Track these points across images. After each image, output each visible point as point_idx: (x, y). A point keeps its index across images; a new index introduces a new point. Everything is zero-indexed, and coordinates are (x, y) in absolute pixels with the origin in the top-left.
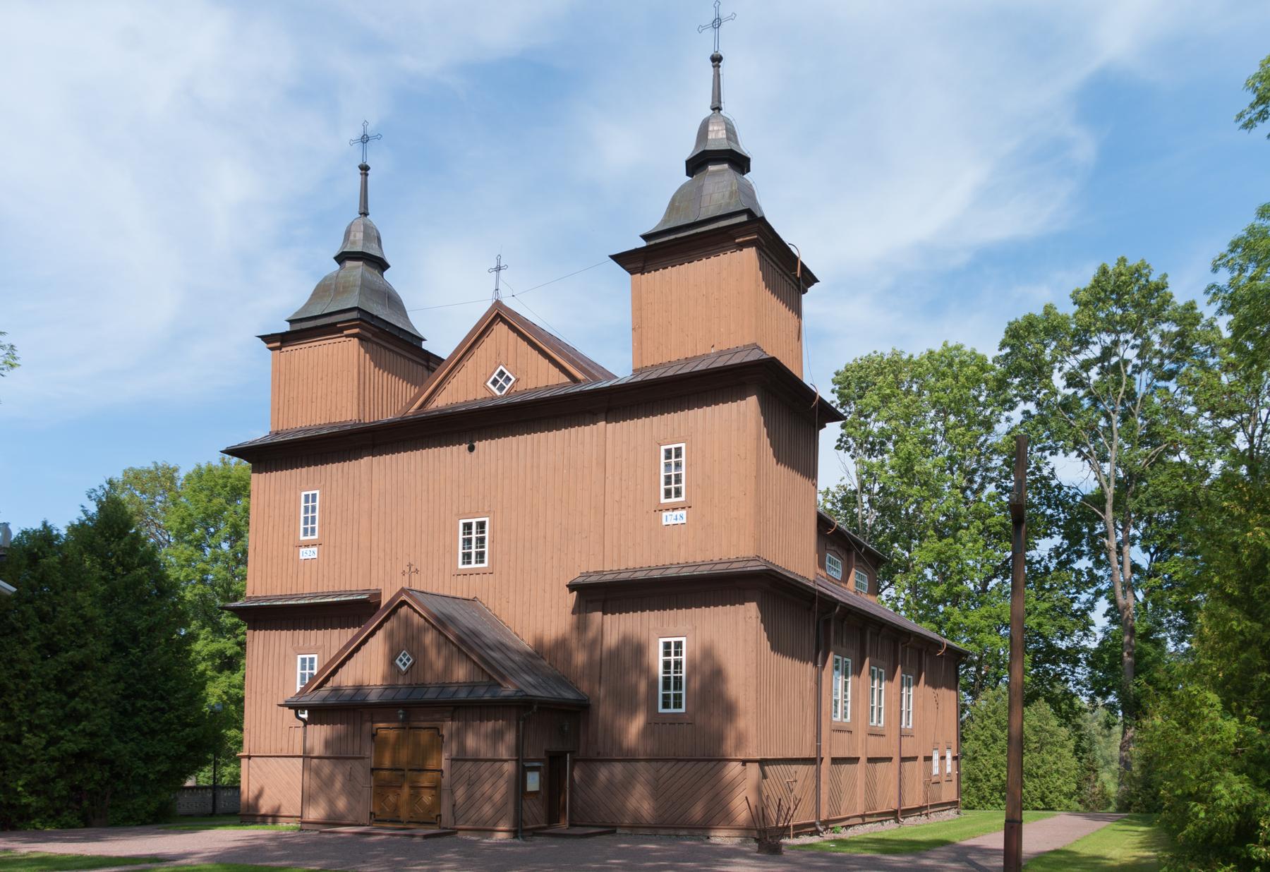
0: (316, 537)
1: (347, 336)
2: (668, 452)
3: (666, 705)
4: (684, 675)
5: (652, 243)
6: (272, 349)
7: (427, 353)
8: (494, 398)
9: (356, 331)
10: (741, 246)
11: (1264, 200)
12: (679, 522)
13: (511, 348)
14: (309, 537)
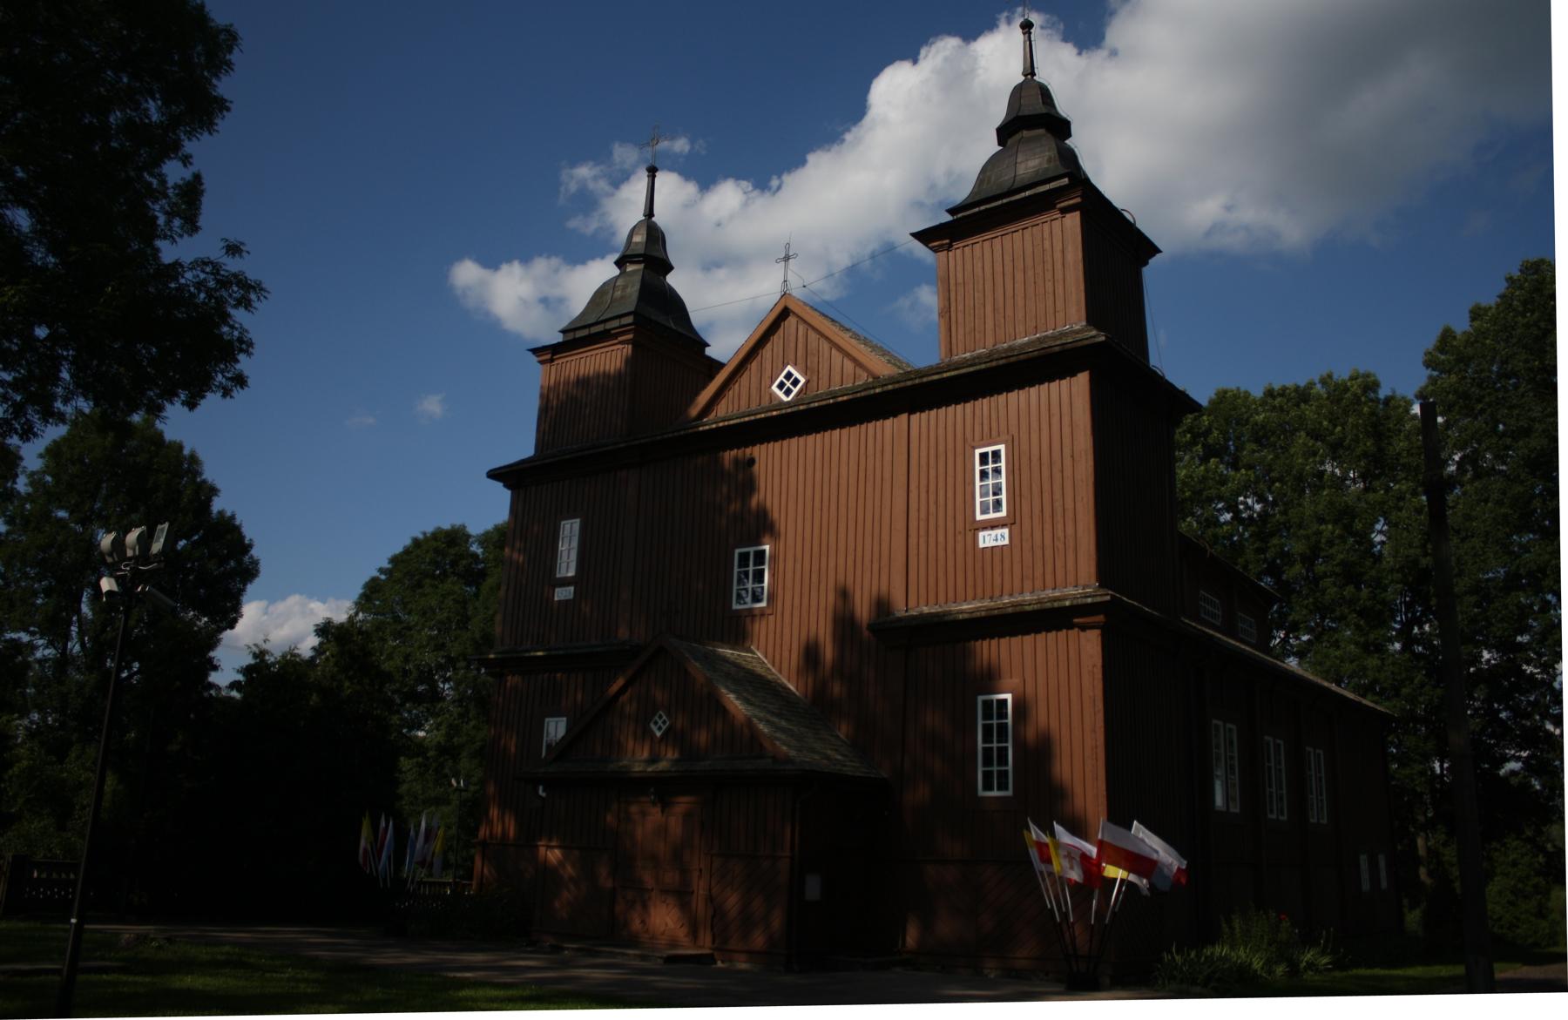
0: (1003, 513)
2: (984, 457)
3: (988, 787)
4: (1010, 720)
6: (541, 362)
7: (709, 359)
8: (782, 404)
10: (1064, 211)
12: (1000, 543)
13: (801, 339)
14: (992, 515)
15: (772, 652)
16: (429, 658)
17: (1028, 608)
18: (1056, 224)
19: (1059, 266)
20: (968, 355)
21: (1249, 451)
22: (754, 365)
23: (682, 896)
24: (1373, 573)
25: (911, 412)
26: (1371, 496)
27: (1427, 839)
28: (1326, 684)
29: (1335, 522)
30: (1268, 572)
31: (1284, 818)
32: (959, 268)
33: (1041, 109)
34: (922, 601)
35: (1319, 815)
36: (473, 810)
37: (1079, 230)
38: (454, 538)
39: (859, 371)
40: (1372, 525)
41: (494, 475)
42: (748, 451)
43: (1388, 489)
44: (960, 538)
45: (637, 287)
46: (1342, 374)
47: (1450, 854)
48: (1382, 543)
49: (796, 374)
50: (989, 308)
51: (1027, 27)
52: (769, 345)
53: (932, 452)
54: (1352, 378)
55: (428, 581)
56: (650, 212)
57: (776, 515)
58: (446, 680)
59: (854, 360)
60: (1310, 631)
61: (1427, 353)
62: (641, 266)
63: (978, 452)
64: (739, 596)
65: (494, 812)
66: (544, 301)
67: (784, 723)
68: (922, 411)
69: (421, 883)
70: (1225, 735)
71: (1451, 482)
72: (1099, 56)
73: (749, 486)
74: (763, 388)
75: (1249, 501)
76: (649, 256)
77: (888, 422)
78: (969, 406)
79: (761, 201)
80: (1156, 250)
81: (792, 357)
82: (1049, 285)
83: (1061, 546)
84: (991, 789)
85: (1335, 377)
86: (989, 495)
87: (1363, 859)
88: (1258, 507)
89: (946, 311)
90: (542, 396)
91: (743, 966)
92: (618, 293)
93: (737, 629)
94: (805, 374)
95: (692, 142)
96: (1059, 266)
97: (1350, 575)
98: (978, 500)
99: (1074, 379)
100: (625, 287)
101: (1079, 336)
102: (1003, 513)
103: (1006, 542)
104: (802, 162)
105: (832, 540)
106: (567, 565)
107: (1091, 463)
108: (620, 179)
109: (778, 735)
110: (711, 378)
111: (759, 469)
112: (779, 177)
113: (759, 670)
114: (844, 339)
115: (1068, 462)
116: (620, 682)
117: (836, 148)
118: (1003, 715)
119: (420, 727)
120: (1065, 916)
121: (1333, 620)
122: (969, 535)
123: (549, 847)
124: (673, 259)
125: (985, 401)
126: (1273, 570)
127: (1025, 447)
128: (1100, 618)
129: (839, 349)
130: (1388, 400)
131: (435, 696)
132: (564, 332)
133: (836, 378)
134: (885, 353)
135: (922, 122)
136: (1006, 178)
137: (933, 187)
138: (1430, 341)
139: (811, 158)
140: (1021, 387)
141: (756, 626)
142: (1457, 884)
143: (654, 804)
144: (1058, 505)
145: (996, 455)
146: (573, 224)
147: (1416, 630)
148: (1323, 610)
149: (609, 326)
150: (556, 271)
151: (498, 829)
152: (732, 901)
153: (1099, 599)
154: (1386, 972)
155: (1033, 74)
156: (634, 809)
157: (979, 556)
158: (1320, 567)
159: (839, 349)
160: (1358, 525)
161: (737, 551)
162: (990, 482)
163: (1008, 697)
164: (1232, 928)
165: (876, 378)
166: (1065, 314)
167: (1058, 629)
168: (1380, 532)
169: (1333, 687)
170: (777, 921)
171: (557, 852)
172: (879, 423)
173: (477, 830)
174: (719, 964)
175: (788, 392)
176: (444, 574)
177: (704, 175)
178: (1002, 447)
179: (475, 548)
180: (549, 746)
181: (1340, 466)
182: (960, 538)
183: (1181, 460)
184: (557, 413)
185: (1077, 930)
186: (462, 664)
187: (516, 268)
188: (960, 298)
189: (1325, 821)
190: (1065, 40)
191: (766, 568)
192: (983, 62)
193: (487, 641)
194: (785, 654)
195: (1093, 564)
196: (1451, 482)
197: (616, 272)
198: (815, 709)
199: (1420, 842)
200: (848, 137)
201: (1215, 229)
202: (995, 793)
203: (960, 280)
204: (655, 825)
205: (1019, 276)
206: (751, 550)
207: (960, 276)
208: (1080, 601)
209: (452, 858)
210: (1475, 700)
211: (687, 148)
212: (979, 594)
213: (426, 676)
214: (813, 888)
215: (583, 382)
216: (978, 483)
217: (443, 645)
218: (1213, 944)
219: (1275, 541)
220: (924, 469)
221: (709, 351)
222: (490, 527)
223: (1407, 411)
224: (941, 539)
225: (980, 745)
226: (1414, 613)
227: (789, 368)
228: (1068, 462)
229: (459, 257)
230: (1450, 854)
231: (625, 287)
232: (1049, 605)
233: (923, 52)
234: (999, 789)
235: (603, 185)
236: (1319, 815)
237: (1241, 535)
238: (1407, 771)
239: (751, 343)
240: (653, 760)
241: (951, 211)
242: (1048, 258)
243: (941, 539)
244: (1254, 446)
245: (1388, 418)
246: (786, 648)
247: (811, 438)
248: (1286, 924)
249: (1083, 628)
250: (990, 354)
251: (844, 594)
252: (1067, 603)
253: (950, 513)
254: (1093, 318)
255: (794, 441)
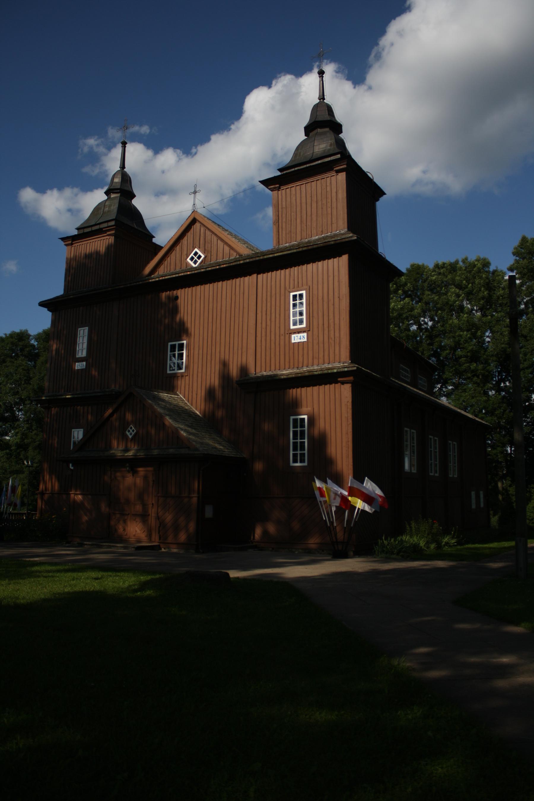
0: (304, 325)
1: (108, 235)
2: (295, 297)
5: (285, 172)
6: (66, 245)
7: (155, 244)
9: (113, 232)
10: (338, 172)
11: (530, 235)
12: (302, 340)
13: (202, 235)
14: (298, 326)
15: (190, 393)
16: (10, 399)
17: (315, 373)
18: (333, 178)
19: (334, 200)
20: (287, 245)
21: (428, 295)
22: (178, 248)
23: (144, 517)
24: (485, 356)
25: (258, 273)
26: (484, 319)
27: (503, 484)
28: (459, 410)
29: (468, 331)
30: (433, 355)
31: (437, 475)
32: (284, 200)
33: (327, 118)
34: (263, 369)
35: (453, 473)
36: (35, 476)
37: (345, 182)
38: (21, 337)
39: (232, 252)
40: (484, 334)
41: (43, 304)
42: (175, 292)
43: (492, 316)
44: (282, 338)
45: (117, 206)
46: (472, 258)
47: (512, 490)
48: (489, 342)
49: (200, 253)
50: (298, 221)
51: (321, 73)
52: (185, 238)
53: (269, 294)
54: (476, 260)
55: (8, 359)
56: (123, 166)
57: (189, 325)
58: (20, 410)
59: (229, 246)
60: (453, 384)
61: (515, 248)
62: (118, 195)
63: (292, 294)
64: (170, 367)
65: (47, 477)
66: (70, 210)
67: (194, 431)
68: (264, 273)
69: (10, 513)
70: (410, 435)
71: (522, 313)
72: (362, 88)
73: (175, 310)
74: (182, 260)
75: (426, 320)
76: (123, 189)
77: (247, 279)
78: (287, 271)
79: (186, 160)
80: (384, 194)
81: (197, 244)
82: (329, 210)
83: (332, 342)
84: (296, 462)
85: (469, 260)
86: (297, 315)
87: (473, 493)
88: (430, 323)
89: (277, 222)
90: (67, 263)
91: (175, 550)
92: (107, 209)
93: (169, 383)
94: (204, 253)
95: (151, 128)
96: (334, 200)
97: (474, 357)
98: (292, 318)
99: (340, 258)
100: (110, 206)
101: (344, 237)
102: (304, 325)
103: (305, 340)
104: (208, 140)
105: (214, 341)
106: (82, 350)
107: (348, 301)
108: (110, 148)
109: (191, 437)
110: (156, 254)
111: (180, 302)
112: (196, 148)
113: (181, 404)
114: (224, 235)
115: (337, 300)
116: (110, 411)
117: (226, 133)
118: (302, 426)
119: (7, 435)
120: (332, 523)
121: (464, 379)
122: (287, 336)
123: (75, 494)
124: (135, 192)
125: (296, 268)
126: (436, 354)
127: (315, 292)
128: (351, 378)
129: (222, 240)
130: (494, 272)
131: (15, 419)
132: (78, 229)
133: (220, 255)
134: (245, 243)
135: (268, 121)
136: (308, 154)
137: (274, 155)
138: (516, 242)
139: (213, 138)
140: (314, 262)
141: (179, 382)
142: (514, 504)
143: (129, 472)
144: (331, 321)
145: (301, 296)
146: (86, 170)
147: (502, 385)
148: (459, 373)
149: (102, 226)
150: (76, 195)
151: (49, 486)
152: (169, 518)
153: (350, 369)
154: (481, 546)
155: (324, 99)
156: (118, 474)
157: (292, 346)
158: (459, 352)
159: (222, 240)
160: (479, 333)
161: (170, 344)
162: (298, 309)
163: (306, 417)
164: (411, 527)
165: (241, 255)
166: (336, 224)
167: (331, 384)
168: (488, 337)
169: (463, 412)
170: (192, 526)
171: (80, 497)
172: (242, 279)
173: (38, 485)
174: (163, 550)
175: (195, 262)
176: (17, 355)
177: (156, 146)
178: (304, 292)
179: (33, 342)
180: (74, 443)
181: (470, 303)
182: (282, 338)
183: (392, 298)
184: (75, 271)
185: (338, 529)
186: (28, 402)
187: (55, 192)
188: (284, 215)
189: (456, 476)
190: (348, 79)
191: (184, 352)
192: (303, 89)
193: (41, 389)
194: (195, 396)
195: (348, 351)
196: (522, 313)
197: (105, 197)
198: (208, 423)
199: (500, 484)
200: (233, 127)
201: (418, 182)
202: (298, 464)
203: (284, 206)
204: (131, 482)
205: (314, 205)
206: (177, 343)
207: (284, 203)
208: (341, 370)
209: (26, 500)
210: (528, 418)
211: (148, 131)
212: (292, 366)
213: (9, 408)
214: (209, 512)
215: (88, 256)
216: (291, 310)
217: (18, 392)
218: (402, 535)
219: (437, 339)
220: (265, 302)
221: (154, 240)
222: (41, 331)
223: (503, 278)
224: (273, 338)
225: (292, 441)
226: (502, 376)
227: (196, 250)
228: (337, 300)
229: (24, 186)
230: (512, 490)
231: (110, 206)
232: (326, 372)
233: (274, 82)
234: (301, 462)
235: (102, 149)
236: (453, 473)
237: (421, 337)
238: (495, 451)
239: (176, 237)
240: (127, 450)
241: (280, 170)
242: (329, 196)
243: (273, 338)
244: (429, 293)
245: (494, 281)
246: (194, 393)
247: (207, 286)
248: (436, 525)
249: (343, 383)
250: (298, 245)
251: (225, 365)
252: (335, 371)
253: (277, 325)
254: (351, 228)
255: (198, 287)
